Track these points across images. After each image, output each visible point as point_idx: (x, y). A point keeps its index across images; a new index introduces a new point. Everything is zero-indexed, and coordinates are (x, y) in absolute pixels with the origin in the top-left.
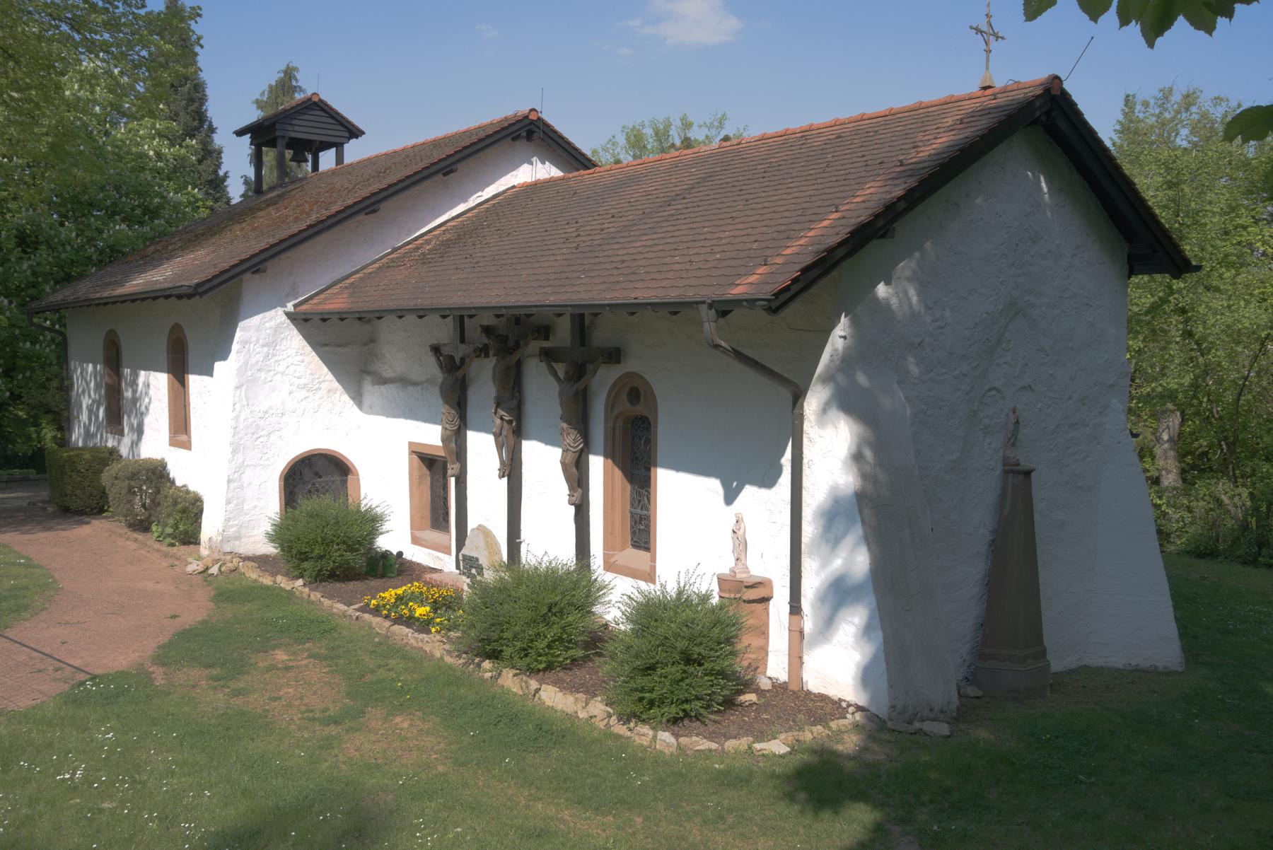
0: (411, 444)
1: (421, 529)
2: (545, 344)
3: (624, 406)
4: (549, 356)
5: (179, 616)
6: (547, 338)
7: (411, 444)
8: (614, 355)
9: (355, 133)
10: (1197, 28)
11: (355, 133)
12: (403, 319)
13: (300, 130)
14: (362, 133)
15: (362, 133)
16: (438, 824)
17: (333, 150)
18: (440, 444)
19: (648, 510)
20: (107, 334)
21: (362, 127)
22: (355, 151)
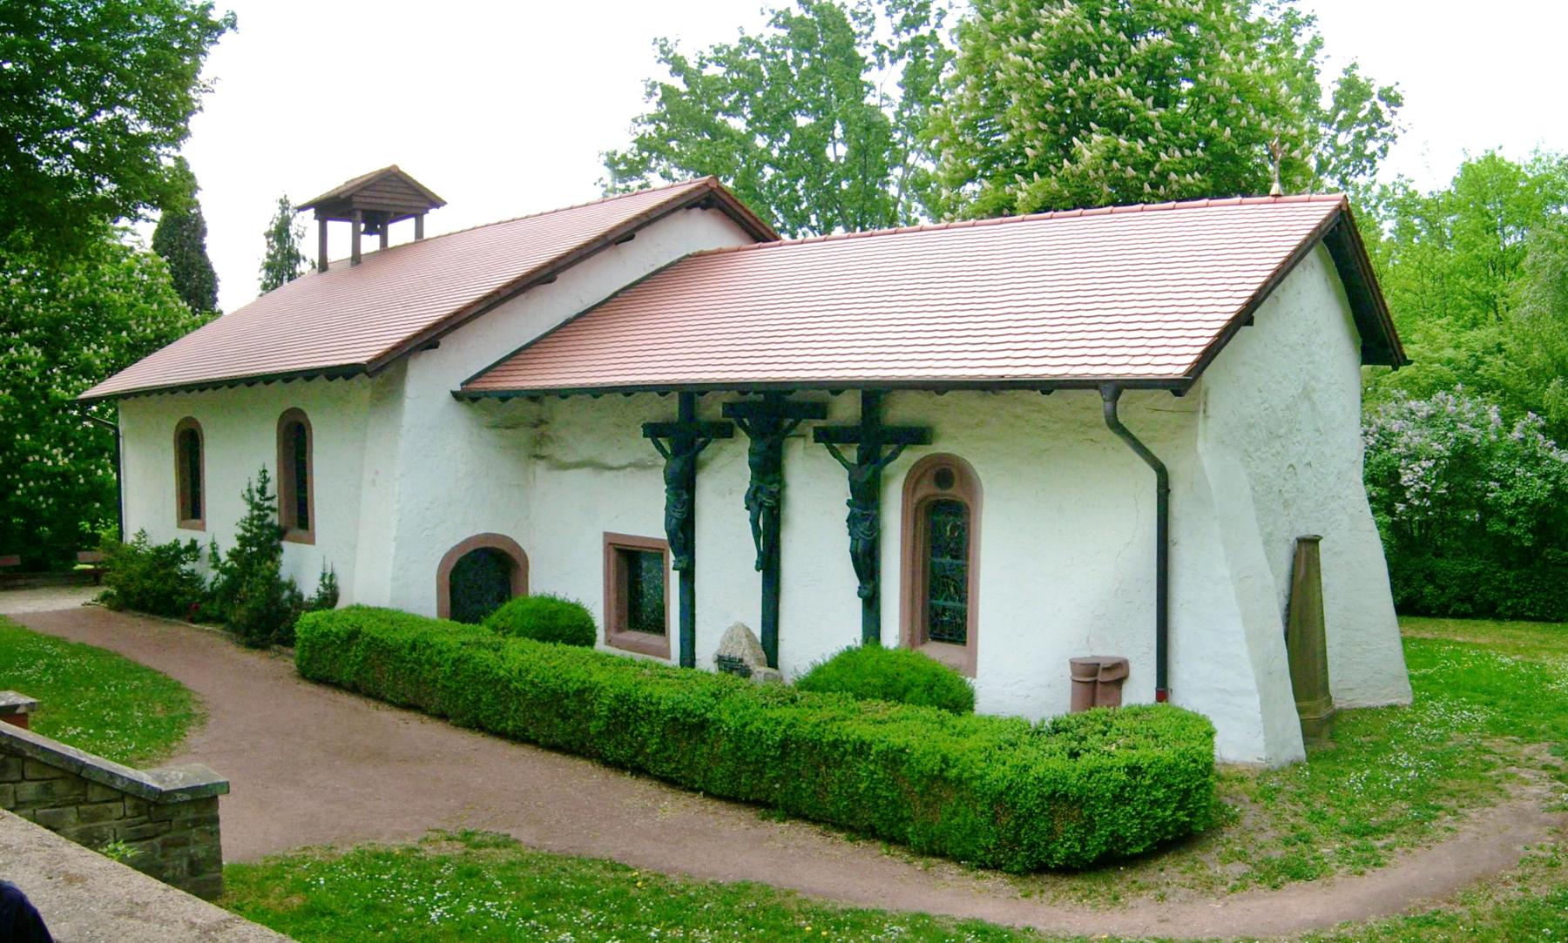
0: (606, 534)
1: (620, 630)
2: (820, 423)
3: (927, 489)
4: (828, 437)
5: (1307, 548)
6: (824, 417)
7: (606, 534)
8: (917, 435)
9: (436, 203)
10: (191, 177)
11: (436, 203)
12: (630, 398)
13: (384, 201)
14: (444, 203)
15: (444, 203)
16: (1487, 757)
17: (412, 220)
18: (664, 536)
19: (963, 600)
20: (282, 417)
21: (443, 198)
22: (434, 222)
